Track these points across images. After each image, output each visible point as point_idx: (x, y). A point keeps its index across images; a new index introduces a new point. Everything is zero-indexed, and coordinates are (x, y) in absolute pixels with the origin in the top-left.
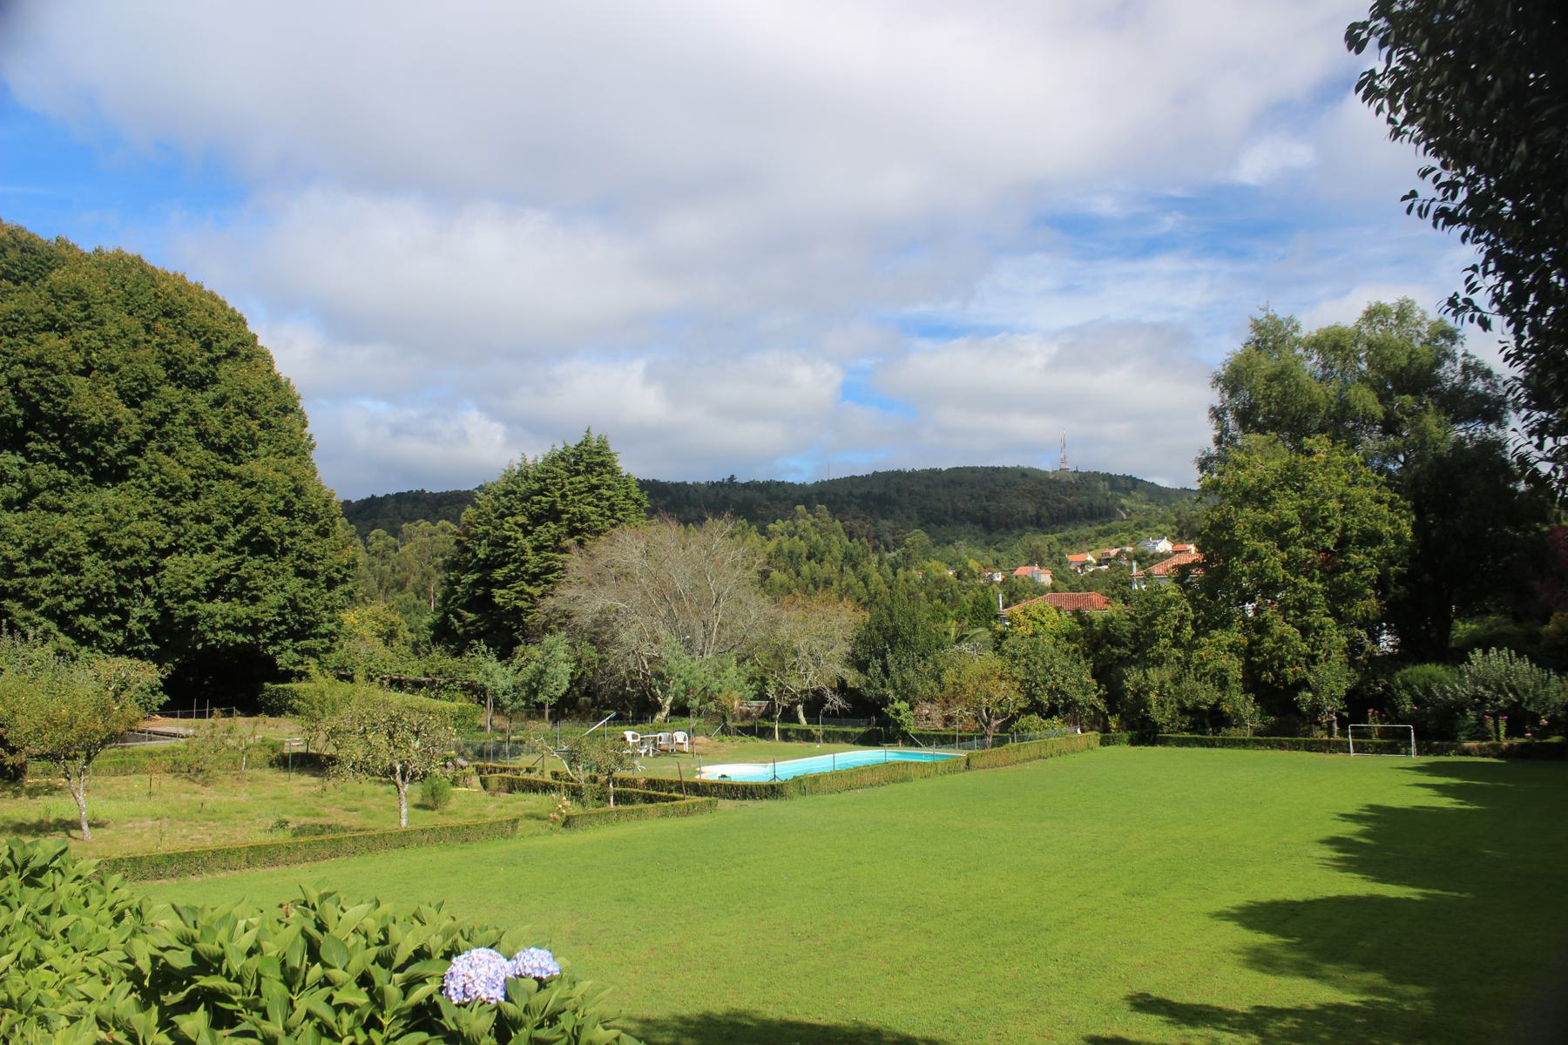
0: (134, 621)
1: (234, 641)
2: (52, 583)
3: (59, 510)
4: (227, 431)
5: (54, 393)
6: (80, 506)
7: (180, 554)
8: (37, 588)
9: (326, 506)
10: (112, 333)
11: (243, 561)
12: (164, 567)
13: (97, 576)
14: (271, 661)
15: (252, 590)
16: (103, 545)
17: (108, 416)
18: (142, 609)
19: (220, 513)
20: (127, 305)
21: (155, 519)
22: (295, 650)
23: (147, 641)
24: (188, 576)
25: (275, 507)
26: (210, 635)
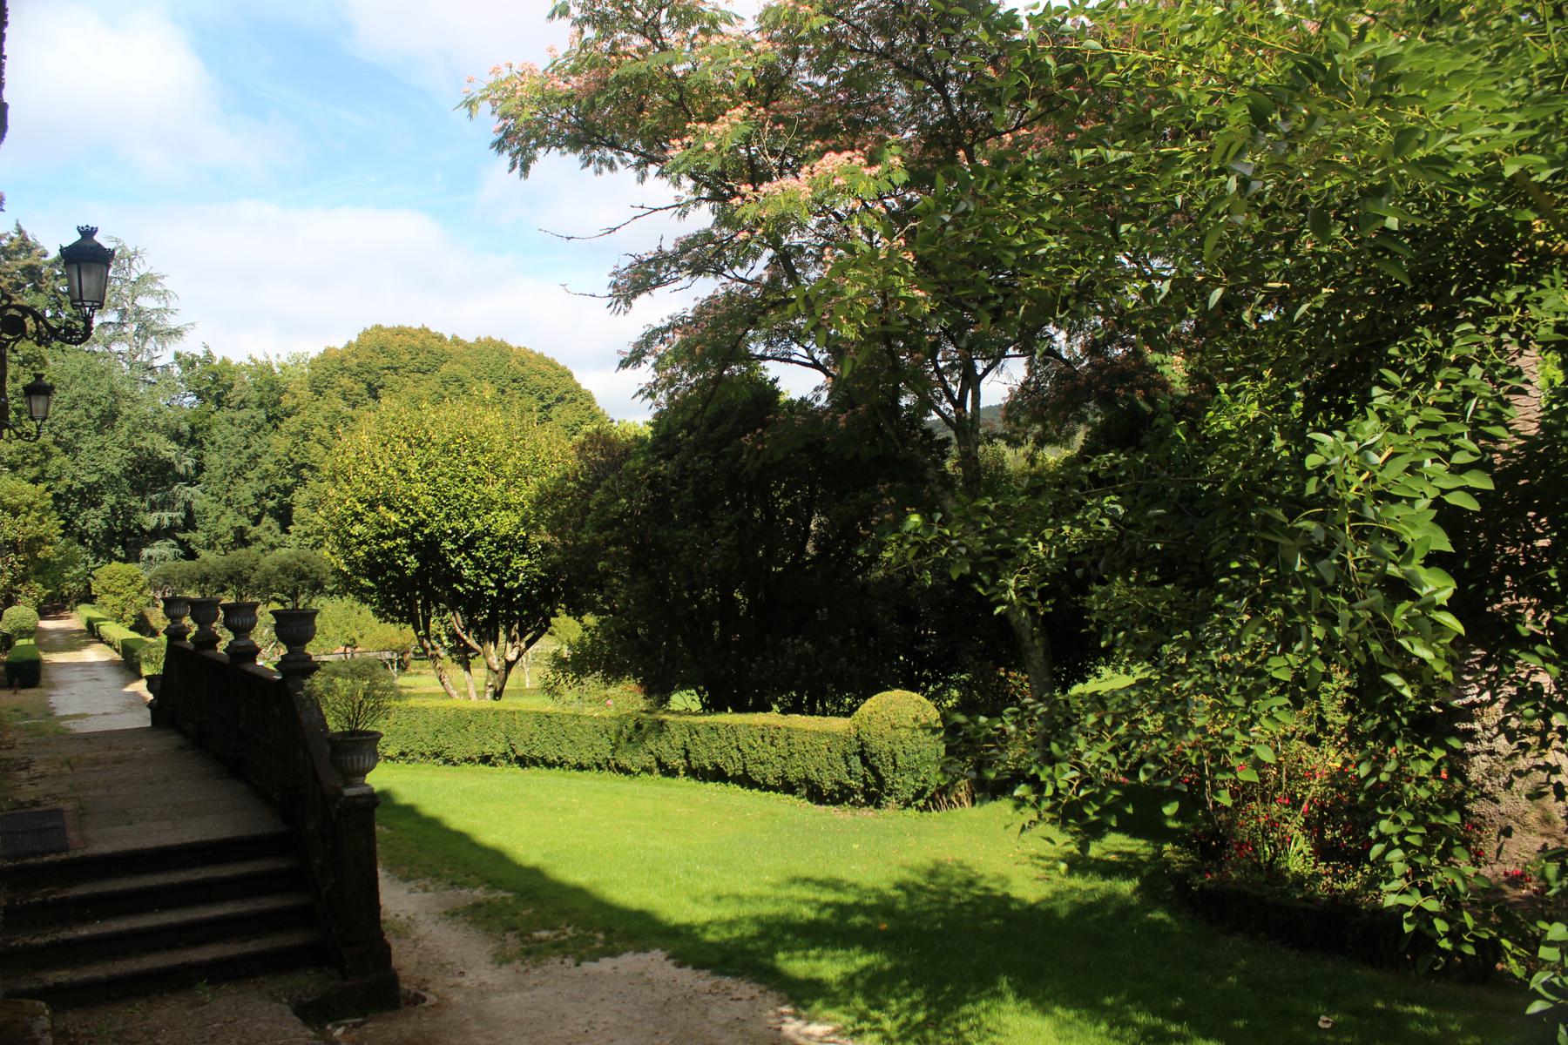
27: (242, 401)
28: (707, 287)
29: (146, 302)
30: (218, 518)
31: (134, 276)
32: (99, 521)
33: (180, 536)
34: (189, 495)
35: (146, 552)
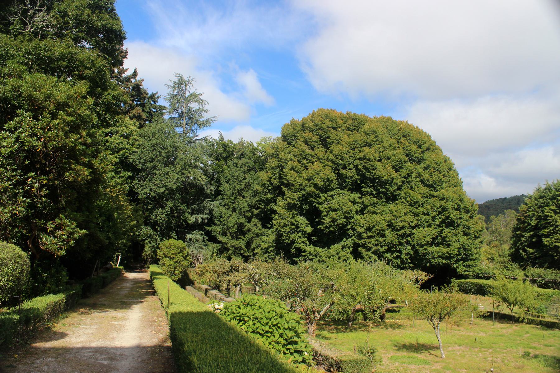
1: (442, 263)
3: (374, 213)
4: (431, 179)
7: (419, 228)
8: (370, 243)
9: (472, 206)
11: (443, 230)
12: (414, 234)
14: (455, 270)
15: (448, 241)
16: (393, 226)
18: (407, 250)
21: (410, 215)
22: (464, 266)
23: (409, 263)
24: (424, 237)
26: (433, 260)
27: (242, 154)
28: (156, 277)
29: (194, 106)
30: (229, 217)
31: (187, 94)
32: (163, 216)
33: (207, 228)
35: (188, 236)
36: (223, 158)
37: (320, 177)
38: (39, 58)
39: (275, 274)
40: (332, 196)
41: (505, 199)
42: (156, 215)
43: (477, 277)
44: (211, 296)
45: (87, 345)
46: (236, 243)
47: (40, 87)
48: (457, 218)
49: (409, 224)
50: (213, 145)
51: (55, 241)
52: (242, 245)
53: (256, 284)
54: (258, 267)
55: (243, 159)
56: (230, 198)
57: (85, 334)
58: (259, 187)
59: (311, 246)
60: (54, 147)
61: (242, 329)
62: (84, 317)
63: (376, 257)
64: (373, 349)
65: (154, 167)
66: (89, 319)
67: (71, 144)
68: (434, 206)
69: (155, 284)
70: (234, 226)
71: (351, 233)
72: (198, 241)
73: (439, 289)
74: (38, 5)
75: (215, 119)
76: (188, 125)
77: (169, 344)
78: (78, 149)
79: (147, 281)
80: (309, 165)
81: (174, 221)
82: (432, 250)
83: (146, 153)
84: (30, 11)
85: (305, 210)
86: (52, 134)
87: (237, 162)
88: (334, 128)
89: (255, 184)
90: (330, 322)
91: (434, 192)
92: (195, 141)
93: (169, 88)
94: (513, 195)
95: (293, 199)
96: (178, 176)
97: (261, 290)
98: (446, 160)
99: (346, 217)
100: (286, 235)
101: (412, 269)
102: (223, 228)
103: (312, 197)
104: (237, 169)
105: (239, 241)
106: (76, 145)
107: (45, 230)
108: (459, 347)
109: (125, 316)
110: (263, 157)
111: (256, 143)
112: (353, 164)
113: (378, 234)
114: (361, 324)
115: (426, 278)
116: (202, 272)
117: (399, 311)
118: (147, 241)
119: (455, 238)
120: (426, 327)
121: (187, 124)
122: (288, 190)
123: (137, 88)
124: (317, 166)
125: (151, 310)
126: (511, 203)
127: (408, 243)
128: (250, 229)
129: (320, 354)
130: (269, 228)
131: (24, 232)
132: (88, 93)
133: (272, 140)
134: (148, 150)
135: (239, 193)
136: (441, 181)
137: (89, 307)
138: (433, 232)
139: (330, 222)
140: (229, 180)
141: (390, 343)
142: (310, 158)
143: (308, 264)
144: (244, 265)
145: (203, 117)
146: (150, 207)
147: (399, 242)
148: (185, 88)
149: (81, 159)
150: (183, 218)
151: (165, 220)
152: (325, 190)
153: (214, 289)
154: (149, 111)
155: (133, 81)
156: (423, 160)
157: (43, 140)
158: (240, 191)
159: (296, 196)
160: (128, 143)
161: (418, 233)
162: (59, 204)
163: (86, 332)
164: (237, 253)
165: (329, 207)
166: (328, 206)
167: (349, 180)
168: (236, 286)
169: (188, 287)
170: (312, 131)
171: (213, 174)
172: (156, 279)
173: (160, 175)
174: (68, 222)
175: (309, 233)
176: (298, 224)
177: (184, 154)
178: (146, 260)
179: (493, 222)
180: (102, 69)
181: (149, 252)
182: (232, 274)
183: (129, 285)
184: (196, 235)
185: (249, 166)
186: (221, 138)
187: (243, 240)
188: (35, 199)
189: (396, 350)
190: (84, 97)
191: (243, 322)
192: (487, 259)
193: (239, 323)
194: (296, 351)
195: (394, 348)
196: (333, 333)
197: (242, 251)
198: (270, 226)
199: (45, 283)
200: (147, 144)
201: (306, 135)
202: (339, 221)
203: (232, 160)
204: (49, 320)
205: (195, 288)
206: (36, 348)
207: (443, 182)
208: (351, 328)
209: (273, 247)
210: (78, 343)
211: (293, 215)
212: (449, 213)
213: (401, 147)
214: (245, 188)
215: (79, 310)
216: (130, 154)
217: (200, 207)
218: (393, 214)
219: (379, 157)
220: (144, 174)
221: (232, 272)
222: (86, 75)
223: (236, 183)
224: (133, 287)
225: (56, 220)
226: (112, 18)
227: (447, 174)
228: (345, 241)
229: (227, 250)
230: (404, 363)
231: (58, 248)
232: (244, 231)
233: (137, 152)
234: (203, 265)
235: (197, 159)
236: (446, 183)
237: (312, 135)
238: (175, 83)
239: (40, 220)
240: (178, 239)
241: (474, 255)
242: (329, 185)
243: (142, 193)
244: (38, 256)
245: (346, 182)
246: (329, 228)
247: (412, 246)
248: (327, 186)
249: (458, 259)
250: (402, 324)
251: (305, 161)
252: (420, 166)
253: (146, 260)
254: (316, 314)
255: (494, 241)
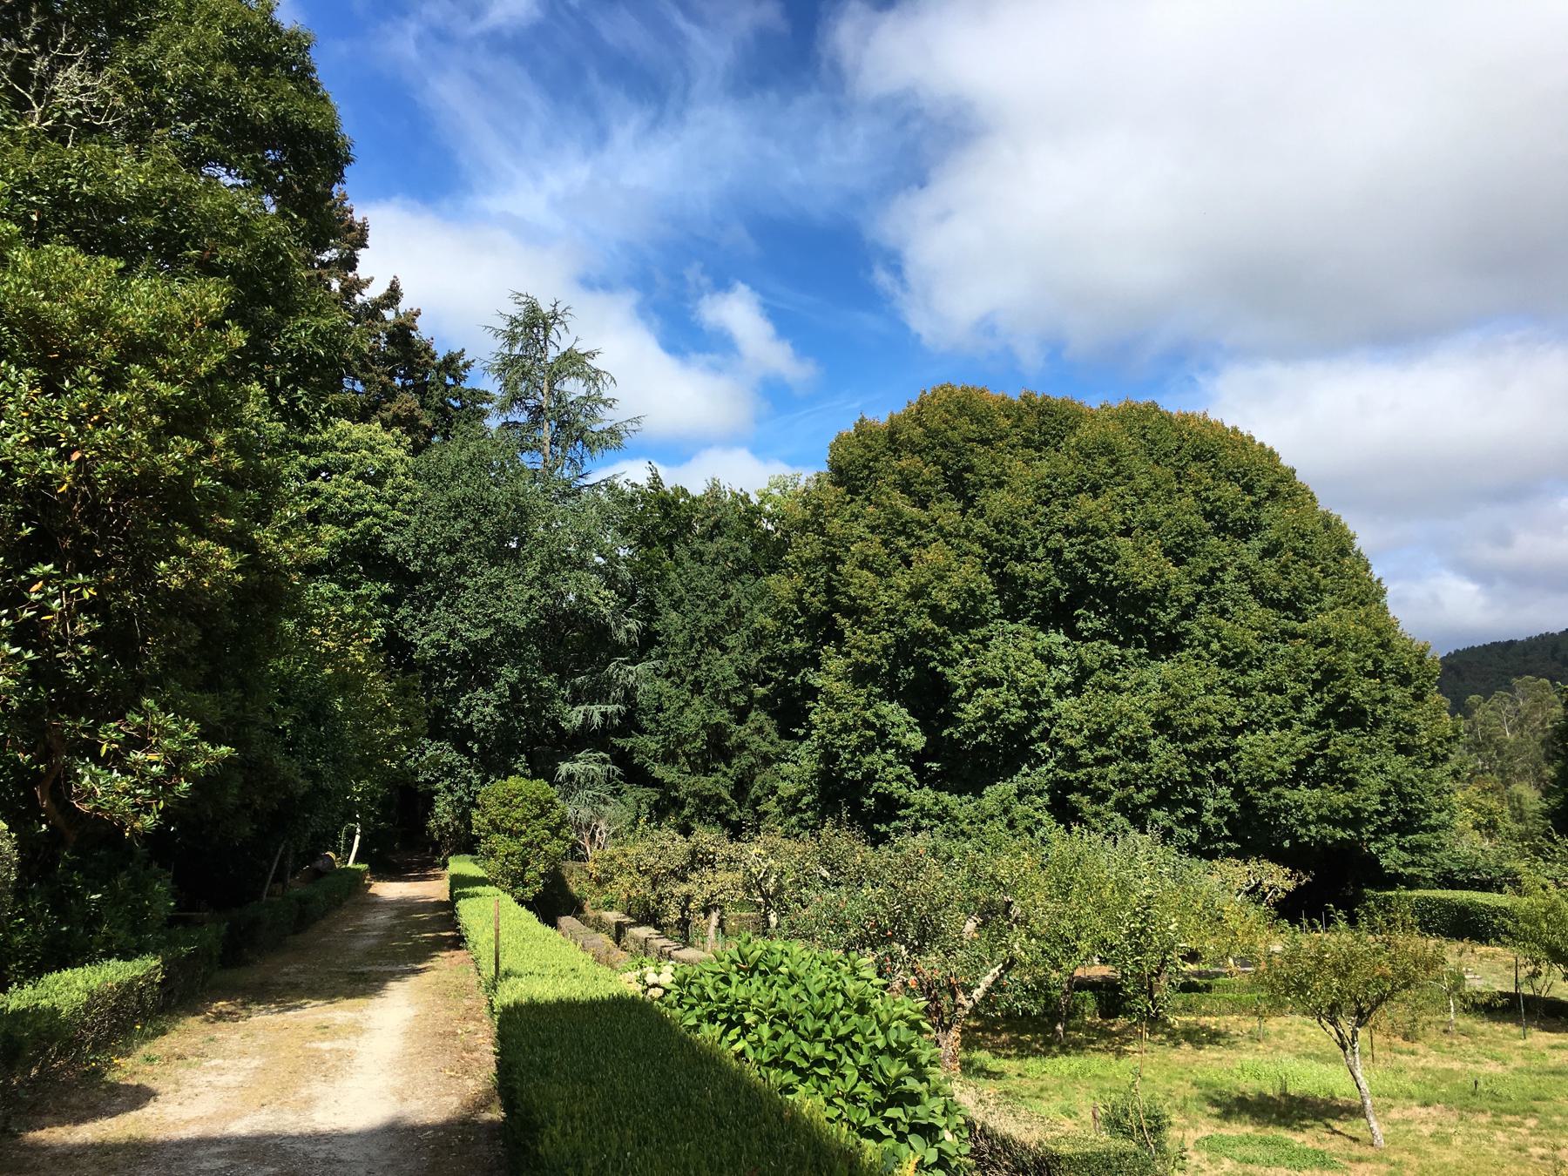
0: (1209, 814)
1: (1332, 838)
2: (1120, 772)
3: (1116, 689)
4: (1286, 582)
5: (1101, 560)
6: (1138, 685)
7: (1253, 733)
8: (1105, 779)
9: (1420, 663)
10: (1144, 486)
11: (1329, 736)
12: (1238, 748)
13: (1167, 762)
14: (1373, 860)
15: (1347, 772)
16: (1170, 726)
17: (1159, 577)
18: (1216, 799)
19: (1294, 681)
20: (1151, 455)
21: (1223, 693)
22: (1402, 848)
23: (1227, 838)
24: (1270, 758)
25: (1363, 668)
26: (1301, 831)
27: (716, 525)
28: (466, 890)
29: (573, 388)
30: (681, 710)
31: (553, 353)
32: (489, 710)
33: (619, 742)
34: (631, 678)
35: (564, 768)
36: (661, 540)
37: (946, 587)
38: (62, 201)
39: (826, 874)
40: (984, 642)
41: (1511, 643)
42: (468, 709)
43: (1448, 881)
44: (632, 946)
45: (216, 1130)
46: (705, 783)
47: (65, 287)
48: (1375, 702)
49: (1222, 720)
50: (632, 501)
51: (124, 782)
52: (721, 789)
53: (767, 904)
54: (772, 851)
55: (720, 540)
56: (683, 653)
57: (215, 1088)
58: (769, 620)
59: (926, 789)
60: (115, 480)
61: (734, 1045)
62: (223, 1030)
63: (1125, 822)
64: (1157, 1118)
65: (461, 568)
66: (237, 1037)
67: (175, 469)
68: (1299, 665)
69: (461, 912)
70: (697, 734)
71: (1043, 751)
72: (593, 780)
73: (1352, 921)
74: (63, 41)
75: (635, 426)
76: (557, 445)
77: (496, 1114)
78: (199, 487)
79: (440, 905)
80: (915, 551)
81: (520, 724)
82: (1296, 798)
83: (435, 526)
84: (38, 61)
85: (906, 681)
86: (109, 437)
87: (701, 548)
88: (984, 442)
89: (756, 611)
90: (996, 1021)
91: (1294, 624)
92: (578, 491)
93: (496, 336)
94: (1536, 631)
95: (870, 652)
96: (532, 592)
97: (784, 921)
98: (1328, 523)
99: (1026, 705)
100: (847, 756)
101: (1242, 855)
102: (664, 740)
103: (924, 644)
104: (704, 569)
105: (713, 779)
106: (190, 476)
107: (91, 750)
108: (1423, 1110)
109: (357, 1021)
110: (778, 534)
111: (757, 493)
112: (1044, 547)
113: (1126, 751)
114: (1094, 1029)
115: (1290, 885)
116: (605, 871)
117: (1208, 988)
118: (439, 785)
119: (1369, 762)
120: (1303, 1040)
121: (554, 442)
122: (852, 626)
123: (402, 334)
124: (936, 554)
125: (445, 995)
126: (1529, 658)
127: (1219, 776)
128: (743, 742)
129: (982, 1130)
130: (802, 739)
131: (24, 758)
132: (230, 313)
133: (802, 483)
134: (441, 518)
135: (711, 639)
136: (1316, 589)
137: (243, 996)
138: (1300, 744)
139: (980, 719)
140: (681, 600)
141: (1195, 1091)
142: (918, 532)
143: (921, 841)
144: (730, 849)
145: (601, 421)
146: (449, 683)
147: (1193, 774)
148: (546, 337)
149: (212, 520)
150: (548, 715)
151: (494, 721)
152: (963, 621)
153: (640, 922)
154: (440, 404)
155: (389, 315)
156: (1258, 528)
157: (76, 456)
158: (714, 631)
159: (877, 641)
160: (379, 499)
161: (1251, 745)
162: (140, 665)
163: (222, 1081)
164: (709, 815)
165: (975, 674)
166: (974, 669)
167: (1035, 593)
168: (706, 911)
169: (566, 921)
170: (920, 452)
171: (633, 586)
172: (466, 896)
173: (477, 591)
174: (168, 721)
175: (917, 752)
176: (884, 725)
177: (547, 526)
178: (440, 843)
179: (1478, 715)
180: (276, 247)
181: (447, 819)
182: (695, 875)
183: (382, 918)
184: (581, 765)
185: (738, 560)
186: (656, 481)
187: (725, 774)
188: (58, 651)
189: (1218, 1117)
190: (216, 324)
191: (738, 1030)
192: (1474, 828)
193: (725, 1033)
194: (915, 1128)
195: (1209, 1109)
196: (1008, 1057)
197: (723, 808)
198: (801, 732)
199: (93, 922)
200: (438, 500)
201: (903, 463)
202: (1006, 715)
203: (687, 544)
204: (96, 1047)
205: (585, 921)
206: (38, 1148)
207: (1324, 591)
208: (1064, 1042)
209: (812, 791)
210: (187, 1122)
211: (867, 698)
212: (1346, 685)
213: (1188, 491)
214: (728, 622)
215: (208, 1008)
216: (386, 529)
217: (598, 682)
218: (1171, 690)
219: (1123, 523)
220: (430, 587)
221: (694, 869)
222: (223, 261)
223: (702, 608)
224: (394, 926)
225: (128, 716)
226: (305, 94)
227: (1333, 566)
228: (1028, 775)
229: (679, 804)
230: (1252, 1162)
231: (136, 805)
232: (727, 748)
233: (408, 523)
234: (608, 850)
235: (586, 543)
236: (1332, 594)
237: (921, 465)
238: (513, 321)
239: (76, 718)
240: (534, 777)
241: (1434, 814)
242: (974, 610)
243: (425, 641)
244: (72, 837)
245: (1025, 597)
246: (975, 735)
247: (1232, 785)
248: (969, 612)
249: (1384, 825)
250: (1222, 1028)
251: (902, 542)
252: (1250, 545)
253: (440, 843)
254: (961, 997)
255: (1482, 772)
